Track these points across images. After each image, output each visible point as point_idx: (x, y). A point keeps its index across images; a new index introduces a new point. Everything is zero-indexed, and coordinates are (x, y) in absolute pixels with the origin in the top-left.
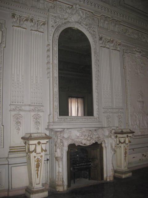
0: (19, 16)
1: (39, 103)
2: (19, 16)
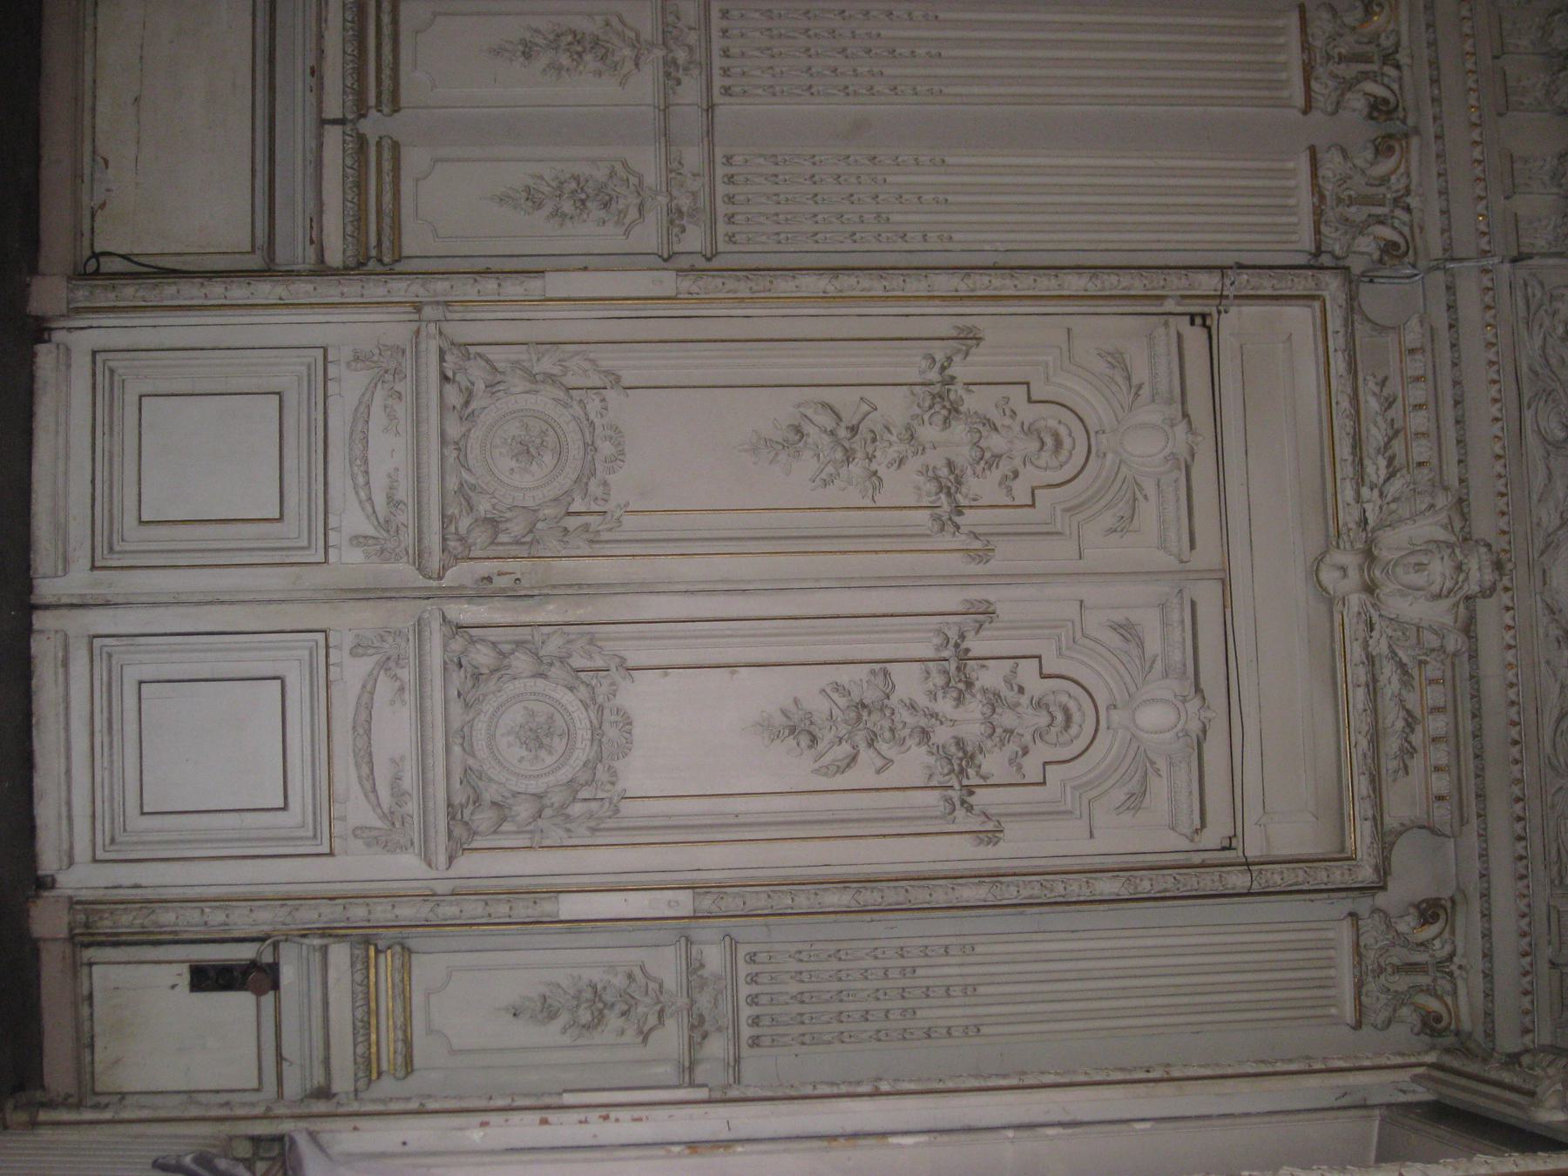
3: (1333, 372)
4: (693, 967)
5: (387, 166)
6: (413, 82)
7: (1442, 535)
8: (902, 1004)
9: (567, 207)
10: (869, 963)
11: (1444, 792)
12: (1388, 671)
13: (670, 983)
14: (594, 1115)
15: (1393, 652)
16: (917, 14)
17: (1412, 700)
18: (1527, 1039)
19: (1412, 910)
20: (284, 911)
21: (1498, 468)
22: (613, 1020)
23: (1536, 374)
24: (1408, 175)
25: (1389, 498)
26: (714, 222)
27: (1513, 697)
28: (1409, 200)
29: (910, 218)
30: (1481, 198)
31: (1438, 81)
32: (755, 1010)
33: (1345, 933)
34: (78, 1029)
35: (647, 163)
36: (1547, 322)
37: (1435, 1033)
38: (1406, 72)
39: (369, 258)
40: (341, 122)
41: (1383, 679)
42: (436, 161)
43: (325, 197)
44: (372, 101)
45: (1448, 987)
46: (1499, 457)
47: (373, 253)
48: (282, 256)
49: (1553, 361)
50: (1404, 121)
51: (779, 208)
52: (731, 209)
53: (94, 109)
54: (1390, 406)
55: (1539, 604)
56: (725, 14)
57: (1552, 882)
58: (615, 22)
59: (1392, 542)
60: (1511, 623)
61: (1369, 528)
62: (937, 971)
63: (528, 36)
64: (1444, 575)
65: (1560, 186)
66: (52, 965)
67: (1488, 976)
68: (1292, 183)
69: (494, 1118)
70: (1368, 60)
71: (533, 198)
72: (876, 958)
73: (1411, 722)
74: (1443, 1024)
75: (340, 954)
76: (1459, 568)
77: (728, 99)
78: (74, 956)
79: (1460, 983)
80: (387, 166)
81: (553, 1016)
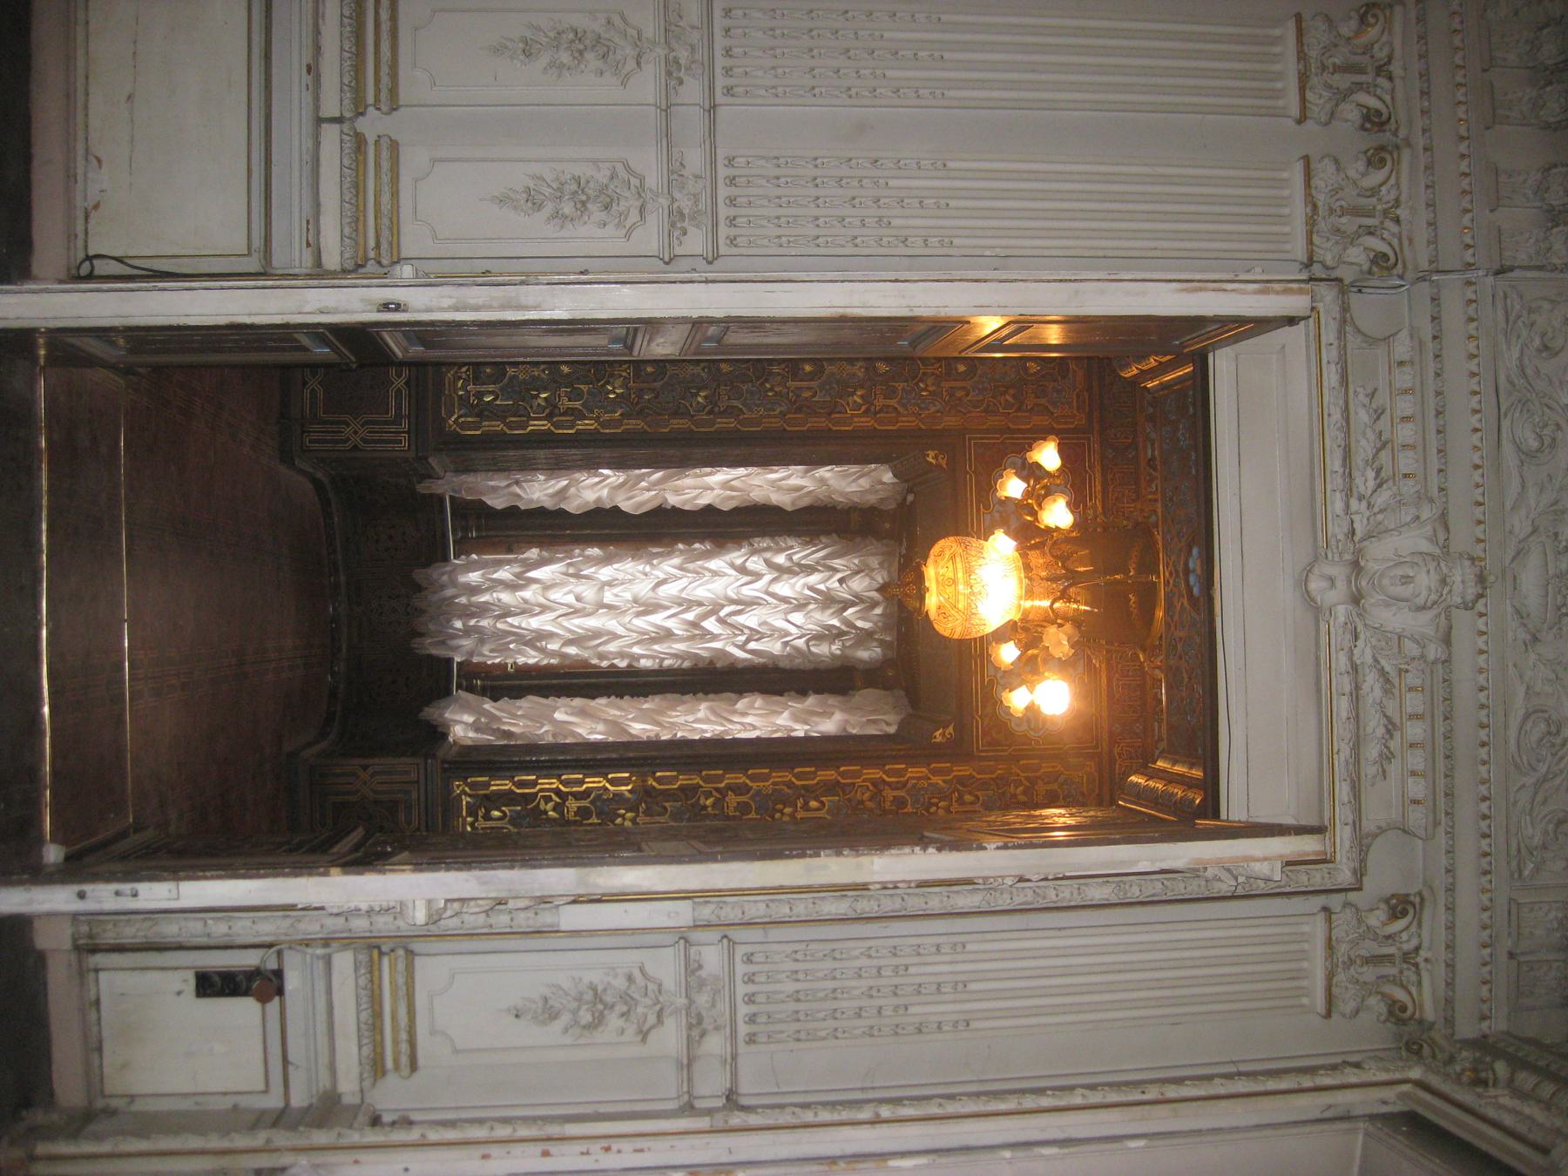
0: (1417, 949)
1: (728, 52)
2: (1417, 949)
3: (1325, 384)
4: (692, 968)
5: (385, 165)
6: (413, 83)
7: (1425, 546)
8: (896, 1001)
9: (567, 209)
10: (864, 962)
11: (1420, 796)
12: (1370, 680)
13: (669, 984)
14: (596, 1147)
15: (1376, 660)
16: (921, 17)
17: (1392, 708)
18: (1485, 1025)
19: (1382, 906)
20: (288, 922)
21: (1477, 477)
22: (614, 1021)
23: (1512, 383)
24: (1398, 185)
25: (1376, 509)
26: (715, 225)
27: (1484, 701)
28: (1398, 212)
29: (911, 222)
30: (1467, 211)
31: (1428, 93)
32: (753, 1009)
33: (1318, 927)
34: (85, 1036)
35: (649, 164)
36: (1524, 333)
37: (1401, 1022)
38: (1398, 82)
39: (367, 260)
40: (339, 120)
41: (1366, 687)
42: (434, 161)
43: (322, 199)
44: (370, 99)
45: (1414, 978)
46: (1477, 467)
47: (372, 254)
48: (278, 260)
49: (1529, 372)
50: (1395, 134)
51: (780, 211)
52: (732, 212)
53: (86, 107)
54: (1378, 418)
55: (1509, 609)
56: (727, 12)
57: (1512, 875)
58: (617, 20)
59: (1379, 552)
60: (1484, 629)
61: (1356, 539)
62: (929, 969)
63: (529, 34)
64: (1430, 589)
65: (1543, 200)
66: (58, 975)
67: (1450, 966)
68: (1286, 192)
69: (494, 1150)
70: (1361, 70)
71: (533, 200)
72: (870, 957)
73: (1391, 728)
74: (1409, 1013)
75: (344, 962)
76: (1444, 582)
77: (730, 100)
78: (80, 962)
79: (1425, 975)
80: (385, 165)
81: (554, 1016)
